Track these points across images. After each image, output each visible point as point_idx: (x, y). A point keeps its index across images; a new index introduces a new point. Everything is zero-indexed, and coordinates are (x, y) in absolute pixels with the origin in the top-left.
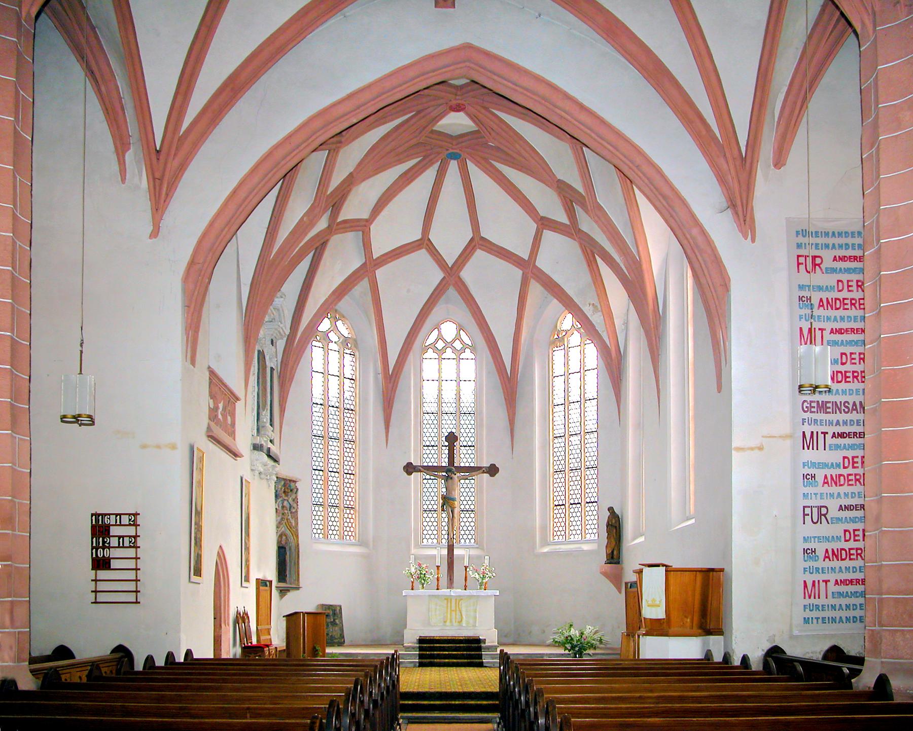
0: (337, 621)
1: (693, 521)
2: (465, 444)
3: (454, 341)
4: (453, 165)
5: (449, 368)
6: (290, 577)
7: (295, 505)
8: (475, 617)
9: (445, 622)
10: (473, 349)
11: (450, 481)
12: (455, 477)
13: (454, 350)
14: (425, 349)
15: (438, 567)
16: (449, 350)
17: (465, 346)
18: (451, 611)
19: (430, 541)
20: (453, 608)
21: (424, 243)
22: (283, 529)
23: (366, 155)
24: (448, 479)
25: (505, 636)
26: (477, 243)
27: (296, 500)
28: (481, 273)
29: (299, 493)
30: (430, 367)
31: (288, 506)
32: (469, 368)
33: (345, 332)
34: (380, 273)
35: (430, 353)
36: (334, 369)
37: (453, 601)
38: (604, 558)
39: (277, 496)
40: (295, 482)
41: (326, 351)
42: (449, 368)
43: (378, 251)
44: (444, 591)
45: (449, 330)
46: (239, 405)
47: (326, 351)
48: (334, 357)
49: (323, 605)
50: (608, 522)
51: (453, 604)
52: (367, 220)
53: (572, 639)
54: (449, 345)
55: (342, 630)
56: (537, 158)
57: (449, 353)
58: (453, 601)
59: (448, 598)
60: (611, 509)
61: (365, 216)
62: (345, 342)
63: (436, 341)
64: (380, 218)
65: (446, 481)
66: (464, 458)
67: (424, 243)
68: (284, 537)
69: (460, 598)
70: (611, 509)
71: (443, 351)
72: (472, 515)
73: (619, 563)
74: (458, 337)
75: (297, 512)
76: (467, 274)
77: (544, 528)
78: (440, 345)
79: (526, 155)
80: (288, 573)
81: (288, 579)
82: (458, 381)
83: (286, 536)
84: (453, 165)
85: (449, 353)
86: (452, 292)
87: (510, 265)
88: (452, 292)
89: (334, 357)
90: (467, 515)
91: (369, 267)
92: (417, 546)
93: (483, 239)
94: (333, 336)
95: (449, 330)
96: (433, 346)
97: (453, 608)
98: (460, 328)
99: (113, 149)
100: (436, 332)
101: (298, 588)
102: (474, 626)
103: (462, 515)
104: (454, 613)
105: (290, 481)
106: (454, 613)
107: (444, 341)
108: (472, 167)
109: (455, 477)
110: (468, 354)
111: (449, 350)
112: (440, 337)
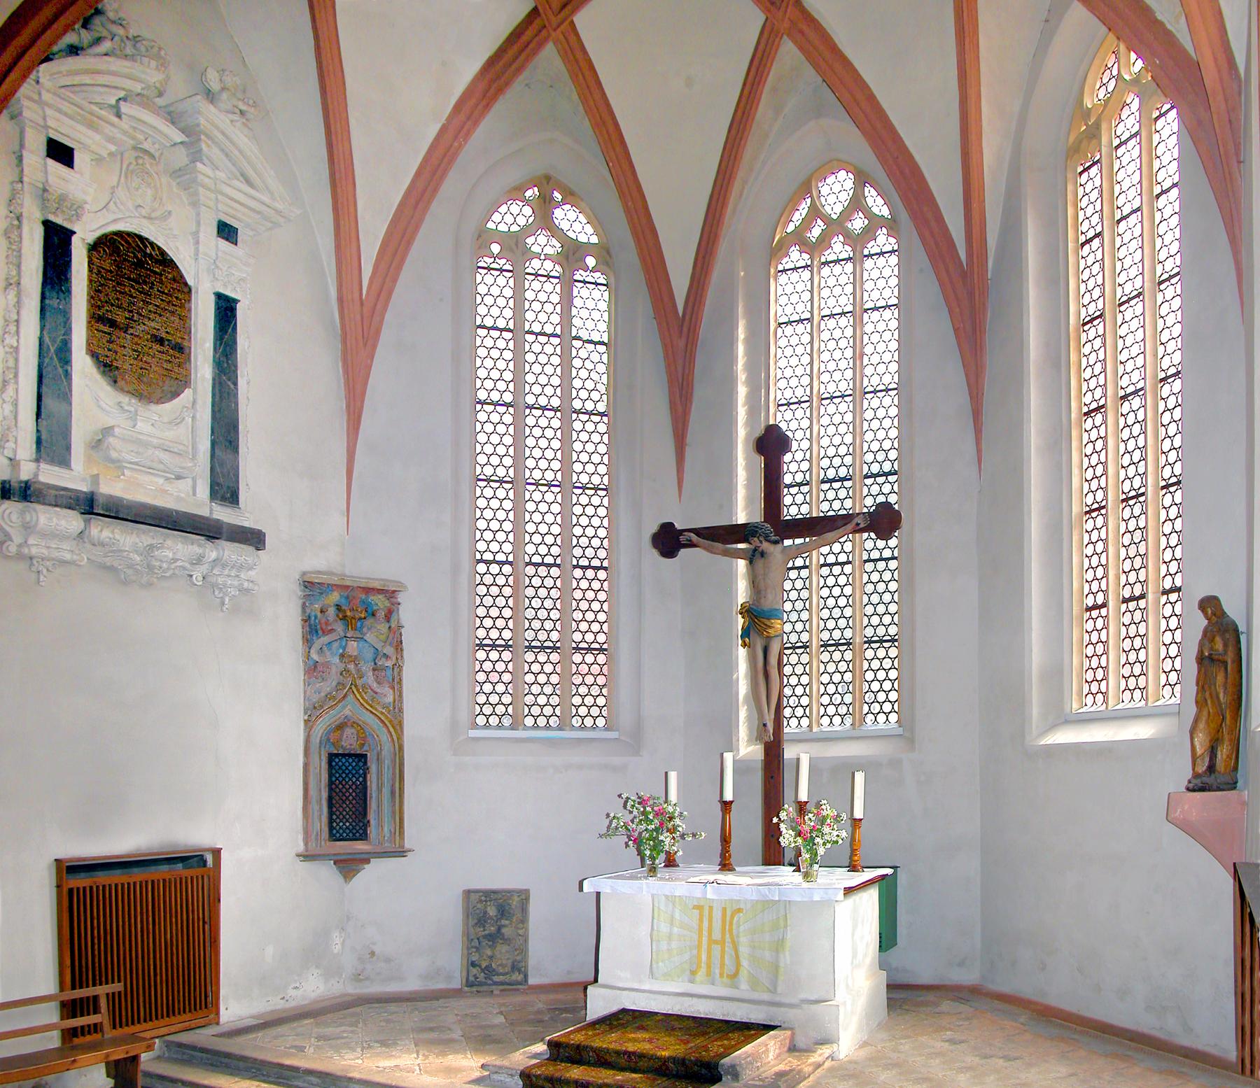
1: (673, 776)
2: (875, 468)
3: (847, 214)
6: (380, 825)
9: (693, 973)
10: (892, 225)
11: (760, 563)
13: (849, 238)
14: (780, 250)
17: (875, 223)
18: (711, 942)
24: (753, 557)
25: (961, 964)
30: (789, 292)
32: (883, 276)
35: (796, 257)
38: (1184, 772)
40: (391, 594)
45: (836, 191)
47: (519, 275)
50: (1201, 652)
54: (836, 226)
55: (523, 950)
57: (839, 248)
60: (1210, 605)
62: (572, 254)
63: (807, 223)
65: (751, 562)
70: (1210, 605)
72: (893, 652)
73: (1232, 785)
74: (857, 204)
75: (398, 667)
77: (1055, 675)
80: (372, 816)
81: (372, 831)
85: (839, 248)
90: (837, 656)
94: (541, 243)
96: (799, 238)
97: (717, 935)
98: (862, 180)
101: (401, 853)
105: (368, 590)
107: (827, 220)
110: (883, 240)
112: (816, 212)
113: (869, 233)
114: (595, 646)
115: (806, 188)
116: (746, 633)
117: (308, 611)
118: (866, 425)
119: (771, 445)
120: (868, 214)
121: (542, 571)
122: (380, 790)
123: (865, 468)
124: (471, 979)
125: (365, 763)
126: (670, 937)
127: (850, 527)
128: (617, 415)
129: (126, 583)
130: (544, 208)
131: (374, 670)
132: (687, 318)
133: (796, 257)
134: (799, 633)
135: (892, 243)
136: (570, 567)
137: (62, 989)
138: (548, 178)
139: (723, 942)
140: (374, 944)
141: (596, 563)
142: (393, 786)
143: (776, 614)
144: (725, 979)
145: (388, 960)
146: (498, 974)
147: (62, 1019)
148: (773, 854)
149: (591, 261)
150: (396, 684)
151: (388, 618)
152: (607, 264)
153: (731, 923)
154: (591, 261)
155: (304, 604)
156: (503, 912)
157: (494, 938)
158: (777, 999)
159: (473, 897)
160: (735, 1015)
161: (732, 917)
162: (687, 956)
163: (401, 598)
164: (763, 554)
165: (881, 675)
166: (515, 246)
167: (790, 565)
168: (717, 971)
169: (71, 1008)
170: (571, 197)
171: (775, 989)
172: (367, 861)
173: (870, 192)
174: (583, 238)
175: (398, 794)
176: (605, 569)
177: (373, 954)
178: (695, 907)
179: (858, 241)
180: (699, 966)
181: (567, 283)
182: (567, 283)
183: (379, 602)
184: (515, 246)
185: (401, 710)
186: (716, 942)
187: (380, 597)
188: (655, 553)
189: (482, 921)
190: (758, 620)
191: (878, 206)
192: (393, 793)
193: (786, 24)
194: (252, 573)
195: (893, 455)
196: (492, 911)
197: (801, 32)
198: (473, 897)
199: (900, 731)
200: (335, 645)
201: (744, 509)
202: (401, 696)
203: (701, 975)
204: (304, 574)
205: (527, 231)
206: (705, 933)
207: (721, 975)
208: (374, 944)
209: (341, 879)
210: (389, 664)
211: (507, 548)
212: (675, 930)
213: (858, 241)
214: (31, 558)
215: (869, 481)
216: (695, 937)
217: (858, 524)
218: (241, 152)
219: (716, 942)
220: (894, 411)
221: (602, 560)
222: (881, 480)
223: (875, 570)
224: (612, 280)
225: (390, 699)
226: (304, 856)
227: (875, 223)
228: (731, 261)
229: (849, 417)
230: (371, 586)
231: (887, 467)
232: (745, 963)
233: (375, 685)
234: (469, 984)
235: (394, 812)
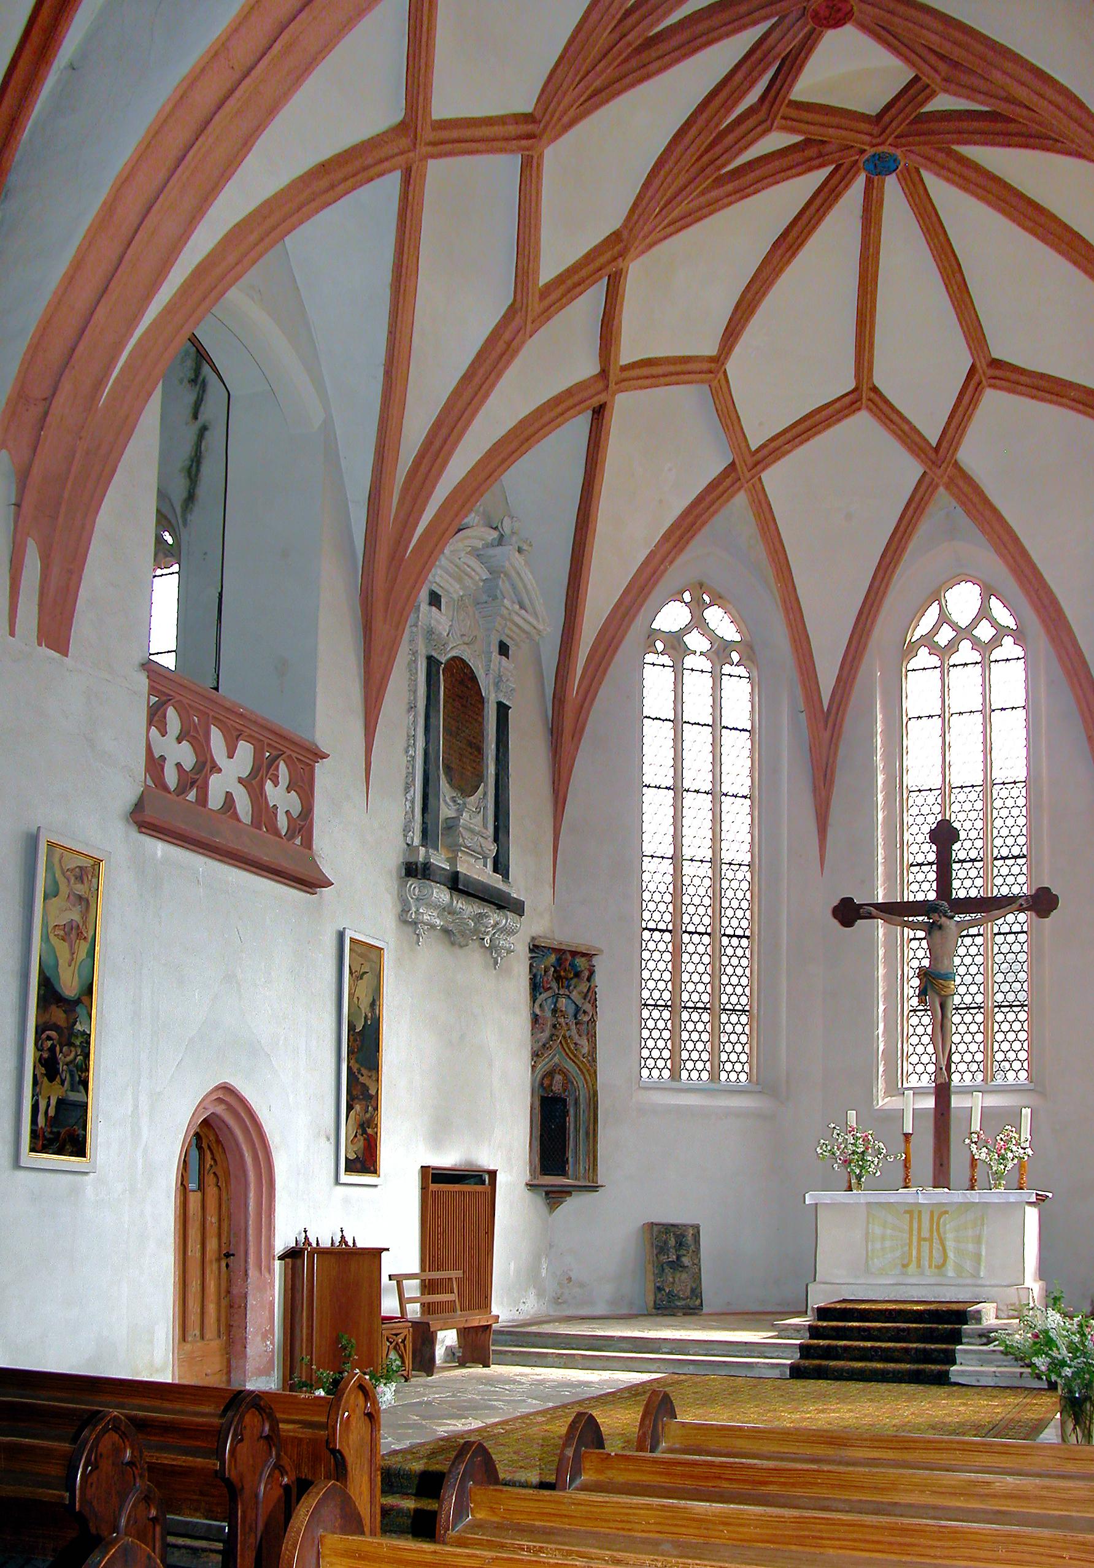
0: (686, 1261)
2: (1004, 852)
3: (975, 623)
4: (892, 186)
5: (965, 685)
7: (587, 1007)
8: (978, 1256)
9: (905, 1266)
10: (1019, 636)
11: (937, 934)
12: (950, 924)
13: (976, 643)
14: (911, 650)
15: (907, 1136)
16: (965, 645)
17: (1001, 631)
18: (921, 1239)
19: (655, 1073)
20: (925, 1234)
21: (864, 396)
22: (556, 1058)
23: (646, 185)
24: (931, 929)
26: (990, 373)
27: (590, 995)
28: (1007, 443)
29: (599, 979)
30: (920, 689)
31: (571, 1010)
32: (1010, 680)
33: (728, 631)
34: (775, 479)
35: (924, 657)
36: (698, 707)
37: (926, 1218)
39: (536, 987)
40: (588, 956)
41: (678, 671)
42: (965, 685)
43: (760, 426)
44: (927, 1196)
45: (963, 600)
46: (322, 773)
47: (678, 671)
48: (698, 686)
49: (652, 1224)
51: (926, 1224)
52: (712, 359)
53: (1050, 1342)
54: (964, 633)
55: (697, 1278)
56: (1049, 93)
57: (966, 652)
58: (926, 1218)
59: (912, 1211)
61: (710, 348)
62: (720, 651)
63: (936, 629)
64: (738, 350)
66: (966, 884)
67: (864, 396)
68: (558, 1078)
69: (939, 1211)
71: (952, 646)
74: (984, 613)
75: (593, 1021)
76: (972, 454)
78: (945, 635)
79: (1022, 93)
80: (570, 1155)
81: (570, 1168)
82: (987, 712)
83: (565, 1074)
84: (892, 186)
85: (966, 652)
86: (943, 500)
87: (342, 44)
88: (943, 500)
89: (698, 686)
91: (744, 470)
92: (888, 1093)
93: (996, 363)
94: (696, 641)
95: (963, 600)
96: (928, 641)
97: (925, 1234)
98: (988, 592)
99: (558, 430)
100: (935, 607)
101: (594, 1188)
102: (976, 1275)
103: (999, 1017)
104: (925, 1245)
105: (574, 954)
106: (925, 1245)
107: (954, 626)
108: (938, 188)
109: (950, 924)
110: (1009, 648)
111: (965, 645)
112: (944, 618)
113: (995, 642)
114: (738, 1007)
115: (937, 596)
116: (922, 993)
117: (534, 970)
118: (995, 812)
119: (944, 835)
120: (994, 623)
121: (1011, 938)
122: (577, 1130)
123: (995, 851)
124: (658, 1302)
125: (565, 1106)
126: (883, 1238)
127: (1015, 906)
128: (762, 798)
129: (453, 944)
130: (697, 608)
131: (576, 1024)
132: (834, 711)
133: (924, 657)
134: (973, 995)
135: (1018, 652)
136: (680, 932)
137: (423, 1269)
138: (701, 585)
139: (930, 1239)
140: (571, 1270)
141: (739, 932)
142: (588, 1127)
143: (949, 976)
144: (933, 1269)
145: (582, 1285)
146: (680, 1298)
147: (423, 1294)
148: (941, 1179)
149: (735, 656)
150: (592, 1037)
151: (589, 980)
152: (749, 658)
153: (938, 1224)
154: (735, 656)
155: (531, 965)
156: (680, 1244)
157: (677, 1265)
158: (980, 1282)
159: (655, 1228)
160: (945, 1296)
161: (939, 1218)
162: (898, 1254)
163: (595, 961)
164: (940, 927)
165: (1011, 1036)
166: (676, 645)
167: (964, 933)
168: (927, 1264)
169: (428, 1287)
170: (718, 600)
171: (979, 1274)
172: (569, 1193)
173: (994, 603)
174: (728, 638)
175: (592, 1135)
176: (748, 937)
177: (570, 1279)
178: (906, 1212)
179: (985, 648)
180: (910, 1260)
181: (717, 678)
182: (717, 678)
183: (580, 962)
184: (676, 645)
185: (594, 1060)
186: (925, 1239)
187: (583, 959)
188: (836, 922)
189: (662, 1249)
190: (934, 983)
191: (1005, 617)
192: (587, 1134)
193: (945, 479)
194: (511, 939)
195: (1022, 840)
196: (672, 1242)
197: (957, 486)
198: (655, 1228)
199: (1032, 1086)
200: (549, 1001)
201: (922, 887)
202: (595, 1048)
203: (912, 1268)
204: (533, 939)
205: (686, 630)
206: (915, 1232)
207: (930, 1266)
208: (571, 1270)
209: (544, 1210)
210: (586, 1019)
211: (707, 920)
212: (889, 1231)
213: (985, 648)
214: (416, 923)
215: (998, 863)
216: (906, 1236)
217: (1021, 905)
218: (525, 587)
219: (925, 1239)
220: (1021, 802)
221: (744, 930)
222: (1010, 862)
223: (1005, 942)
224: (755, 674)
225: (585, 1050)
226: (531, 1185)
227: (1001, 631)
228: (873, 667)
229: (979, 805)
230: (579, 950)
231: (1016, 851)
232: (951, 1254)
233: (577, 1037)
234: (657, 1307)
235: (588, 1151)
